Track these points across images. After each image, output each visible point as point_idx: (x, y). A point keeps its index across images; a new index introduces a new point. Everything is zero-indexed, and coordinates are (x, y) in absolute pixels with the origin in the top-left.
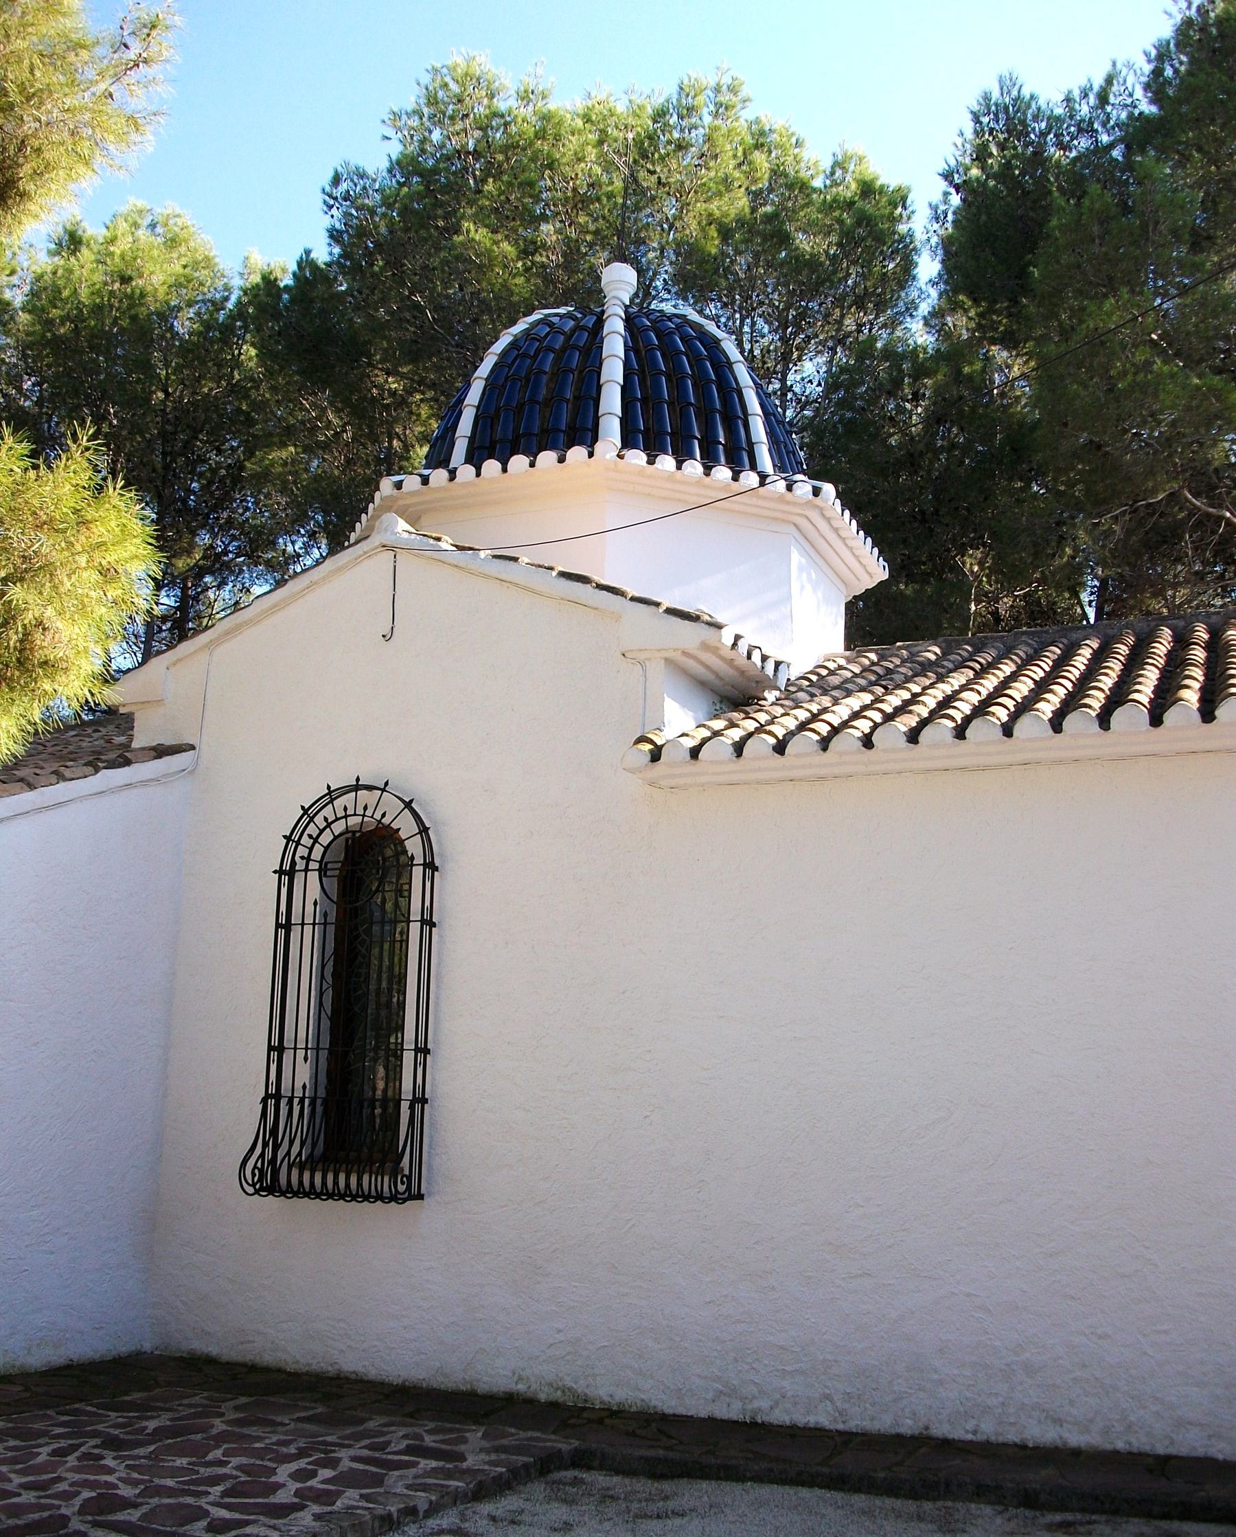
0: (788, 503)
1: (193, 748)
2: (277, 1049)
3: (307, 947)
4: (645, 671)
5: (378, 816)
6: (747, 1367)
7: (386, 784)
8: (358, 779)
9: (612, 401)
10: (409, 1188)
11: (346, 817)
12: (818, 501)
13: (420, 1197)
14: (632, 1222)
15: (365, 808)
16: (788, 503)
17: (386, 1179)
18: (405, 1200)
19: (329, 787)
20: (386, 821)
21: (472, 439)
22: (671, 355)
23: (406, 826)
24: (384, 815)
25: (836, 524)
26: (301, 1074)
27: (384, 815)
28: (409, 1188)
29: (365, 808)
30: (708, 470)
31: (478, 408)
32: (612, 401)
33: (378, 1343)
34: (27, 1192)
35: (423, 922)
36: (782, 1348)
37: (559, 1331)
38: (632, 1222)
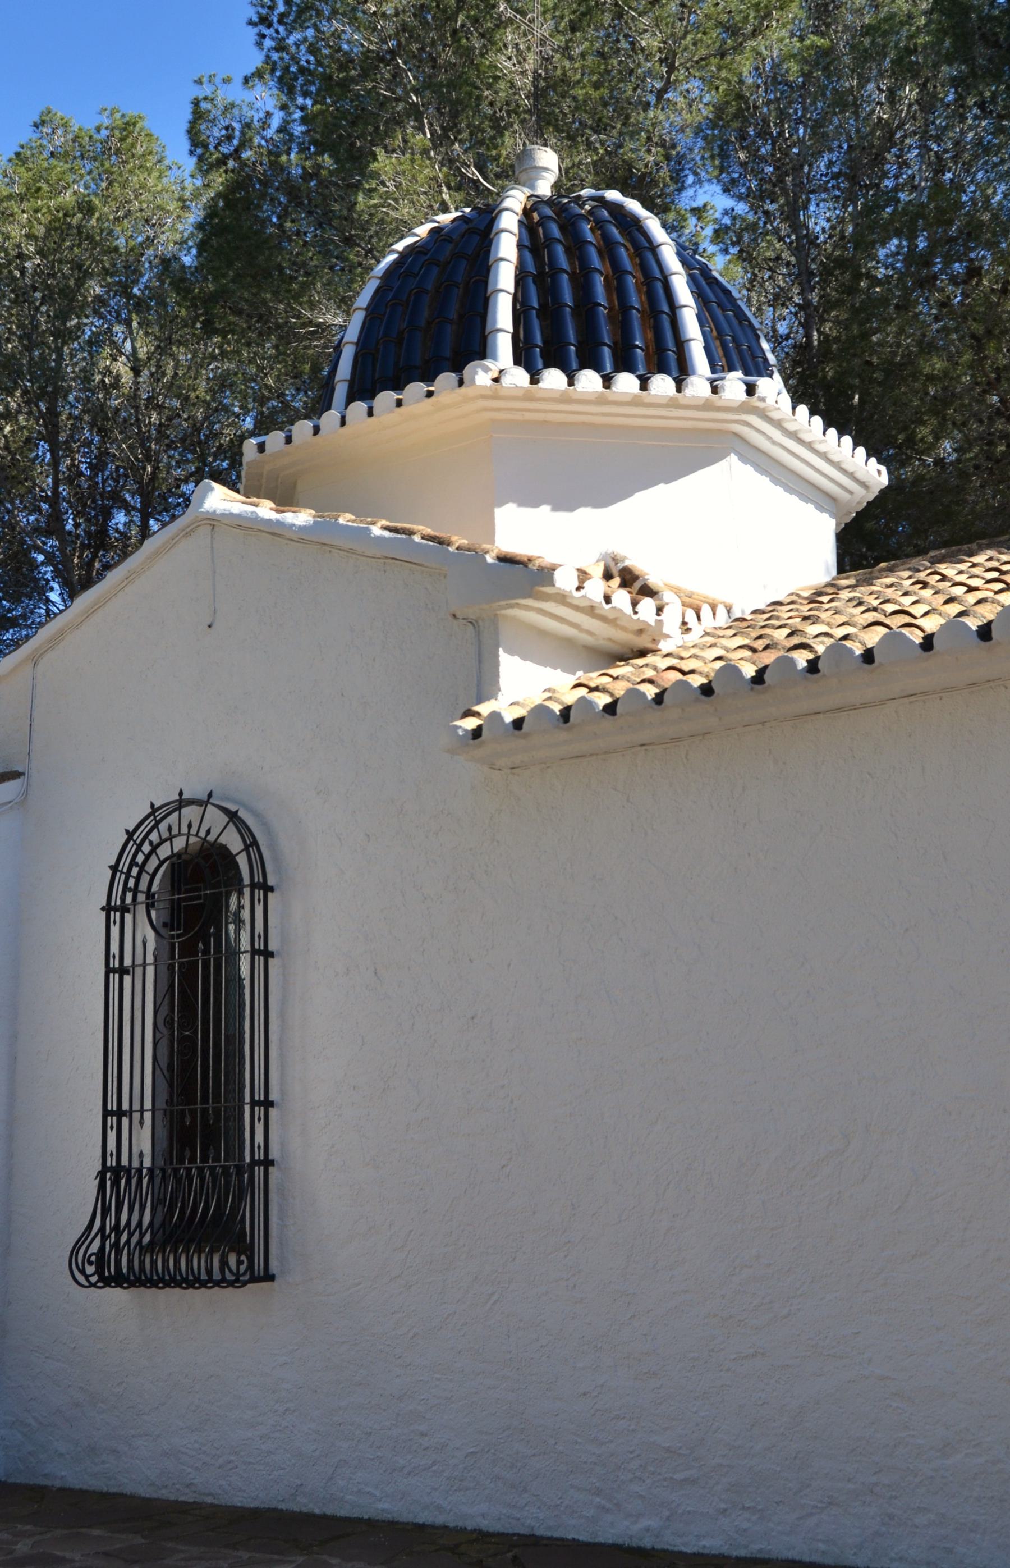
0: (719, 409)
1: (23, 774)
2: (113, 1114)
3: (143, 993)
4: (478, 634)
5: (202, 834)
6: (630, 1476)
7: (210, 795)
8: (181, 793)
9: (503, 313)
10: (251, 1266)
11: (170, 839)
12: (754, 400)
13: (269, 1277)
14: (495, 1298)
15: (190, 826)
16: (719, 409)
17: (203, 1256)
18: (245, 1284)
19: (152, 805)
20: (211, 838)
21: (352, 383)
22: (576, 247)
23: (233, 841)
24: (208, 832)
25: (791, 427)
26: (142, 1142)
27: (208, 832)
28: (251, 1266)
29: (190, 826)
30: (607, 381)
31: (357, 344)
32: (503, 313)
33: (232, 1458)
34: (631, 1453)
35: (254, 952)
36: (668, 1450)
37: (423, 1435)
38: (495, 1298)
